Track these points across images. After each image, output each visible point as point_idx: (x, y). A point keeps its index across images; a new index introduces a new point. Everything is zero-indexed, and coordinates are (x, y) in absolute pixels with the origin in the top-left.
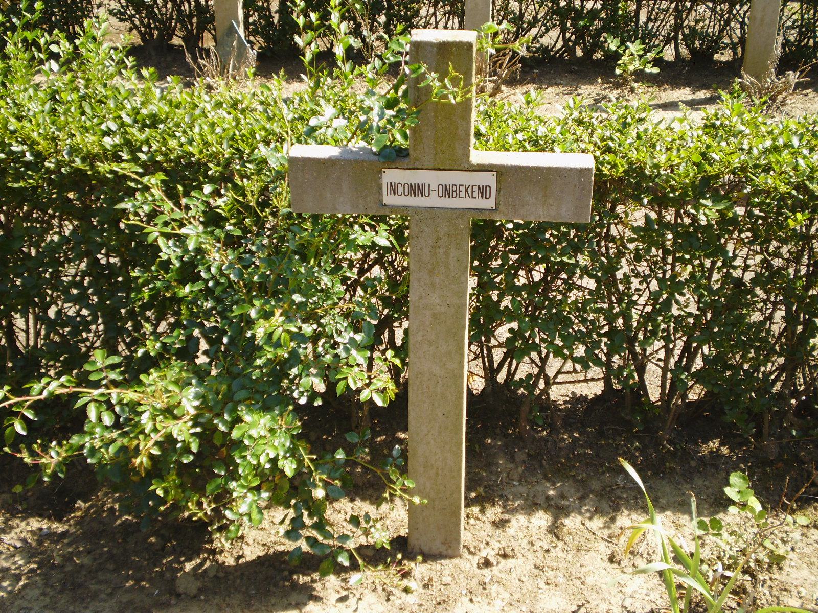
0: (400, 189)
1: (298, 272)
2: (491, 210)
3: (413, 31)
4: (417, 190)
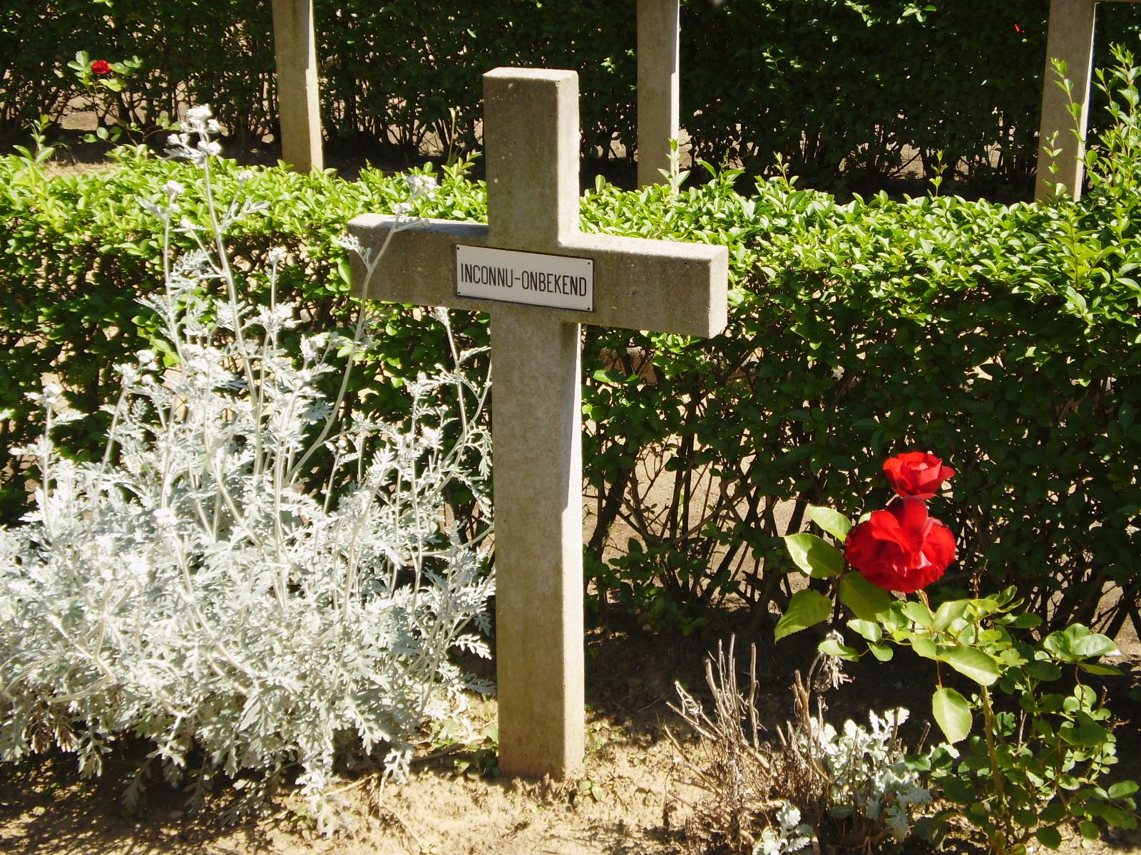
0: (478, 275)
1: (781, 351)
2: (588, 311)
3: (183, 259)
4: (498, 277)
